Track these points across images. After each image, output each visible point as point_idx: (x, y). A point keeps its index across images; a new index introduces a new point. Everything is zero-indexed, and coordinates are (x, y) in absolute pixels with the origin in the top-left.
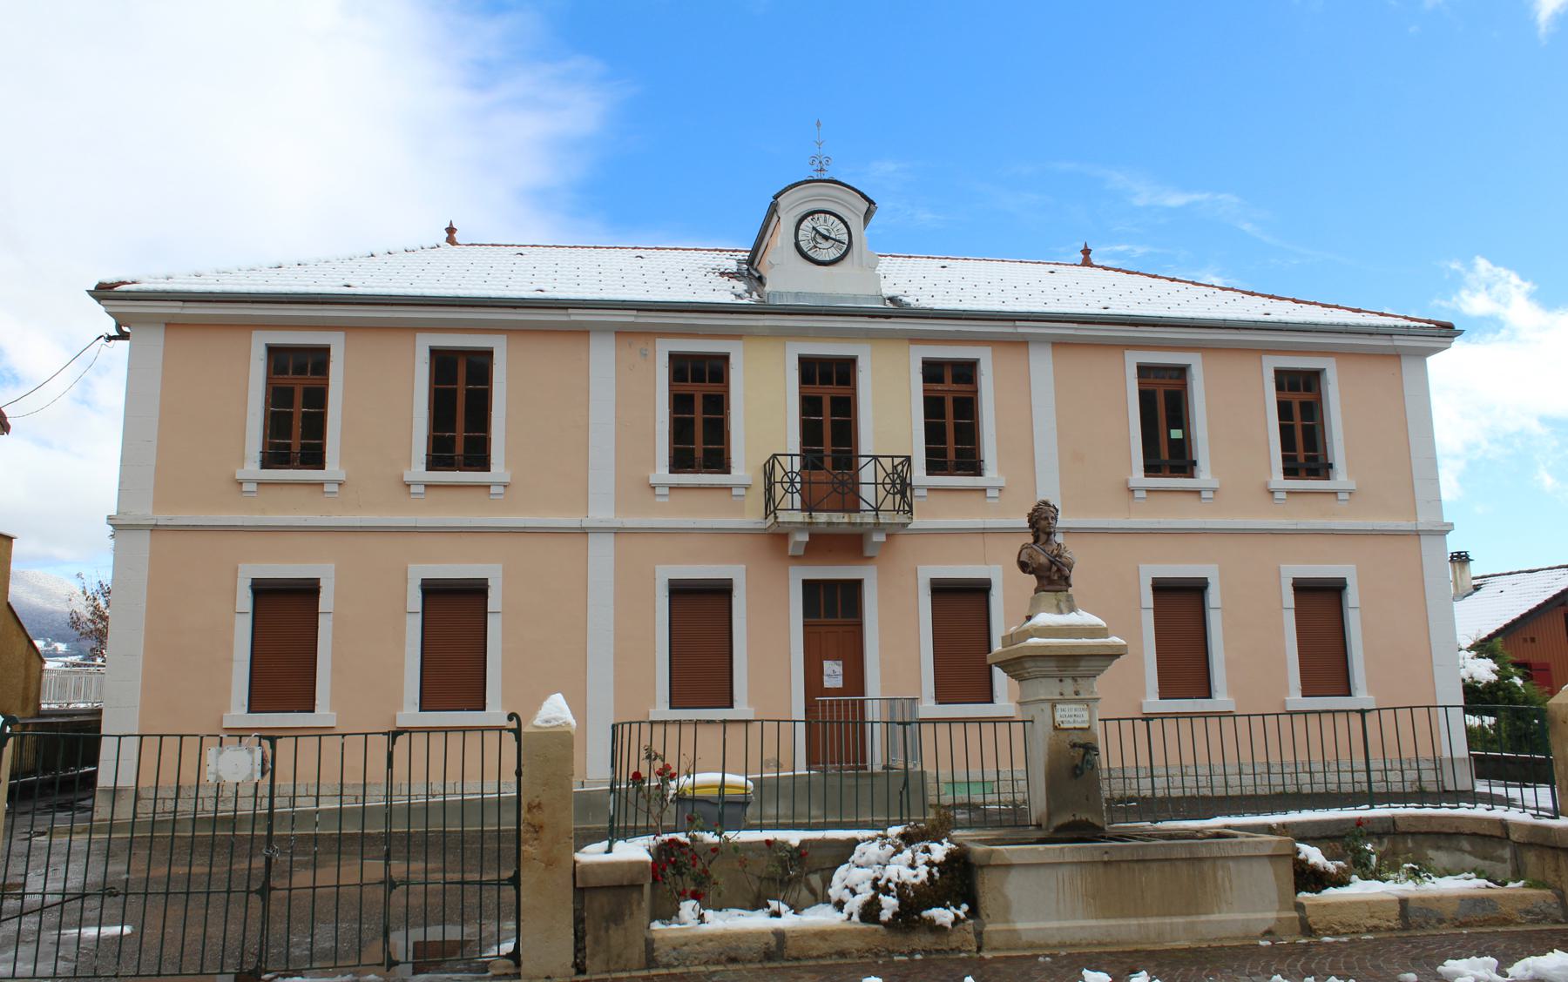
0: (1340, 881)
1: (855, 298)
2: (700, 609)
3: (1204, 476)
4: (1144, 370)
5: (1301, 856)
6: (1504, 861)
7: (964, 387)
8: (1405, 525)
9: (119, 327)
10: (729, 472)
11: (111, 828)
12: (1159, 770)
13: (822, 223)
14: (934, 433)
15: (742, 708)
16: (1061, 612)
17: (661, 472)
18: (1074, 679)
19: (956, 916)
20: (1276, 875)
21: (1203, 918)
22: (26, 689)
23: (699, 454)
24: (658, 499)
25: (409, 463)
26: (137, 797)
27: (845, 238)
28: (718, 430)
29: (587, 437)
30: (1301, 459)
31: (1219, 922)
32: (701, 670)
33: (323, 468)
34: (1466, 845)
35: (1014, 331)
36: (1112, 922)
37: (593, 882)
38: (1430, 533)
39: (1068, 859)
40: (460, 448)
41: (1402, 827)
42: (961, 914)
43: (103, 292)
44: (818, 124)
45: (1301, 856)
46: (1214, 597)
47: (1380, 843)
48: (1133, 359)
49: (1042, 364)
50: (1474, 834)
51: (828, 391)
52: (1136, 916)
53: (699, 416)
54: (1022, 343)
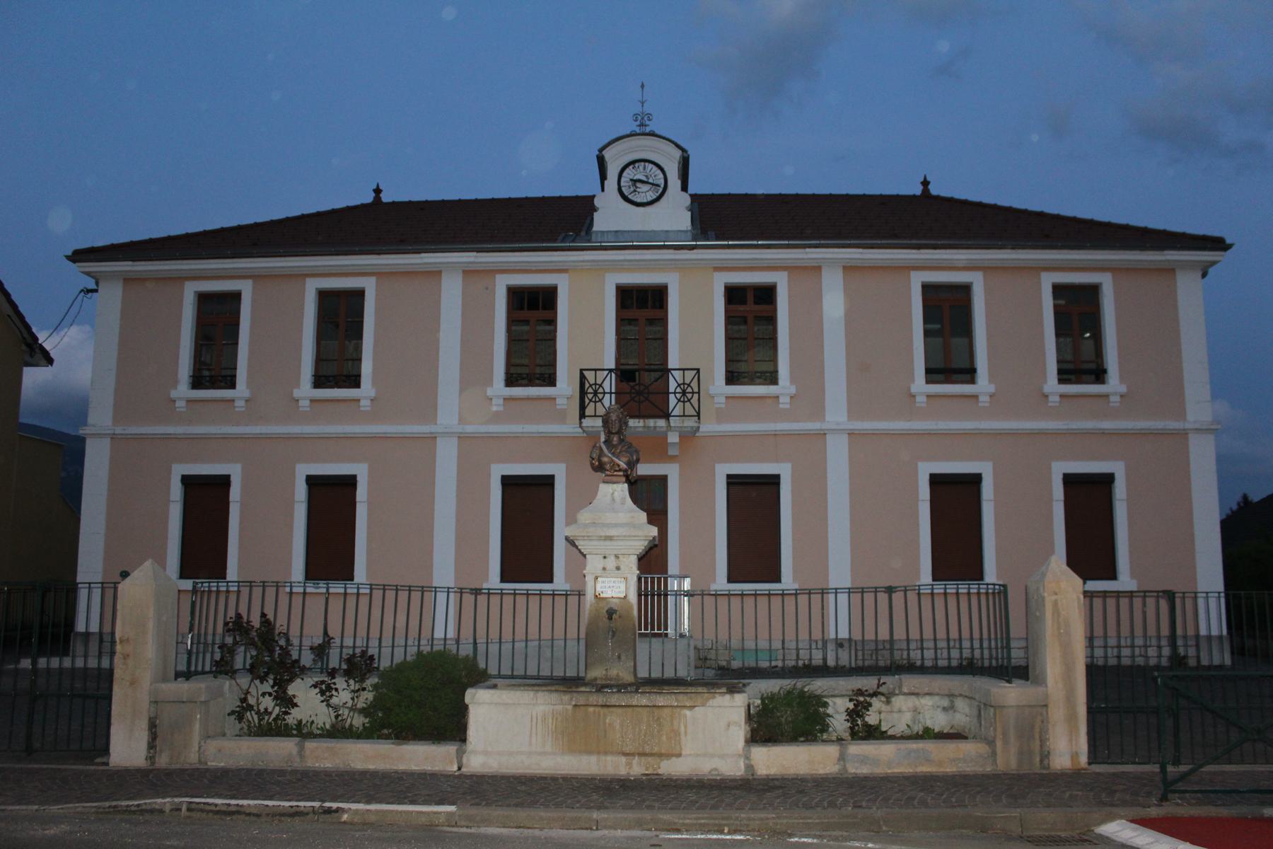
2: (528, 504)
9: (97, 283)
25: (175, 383)
26: (101, 641)
27: (662, 182)
44: (643, 86)
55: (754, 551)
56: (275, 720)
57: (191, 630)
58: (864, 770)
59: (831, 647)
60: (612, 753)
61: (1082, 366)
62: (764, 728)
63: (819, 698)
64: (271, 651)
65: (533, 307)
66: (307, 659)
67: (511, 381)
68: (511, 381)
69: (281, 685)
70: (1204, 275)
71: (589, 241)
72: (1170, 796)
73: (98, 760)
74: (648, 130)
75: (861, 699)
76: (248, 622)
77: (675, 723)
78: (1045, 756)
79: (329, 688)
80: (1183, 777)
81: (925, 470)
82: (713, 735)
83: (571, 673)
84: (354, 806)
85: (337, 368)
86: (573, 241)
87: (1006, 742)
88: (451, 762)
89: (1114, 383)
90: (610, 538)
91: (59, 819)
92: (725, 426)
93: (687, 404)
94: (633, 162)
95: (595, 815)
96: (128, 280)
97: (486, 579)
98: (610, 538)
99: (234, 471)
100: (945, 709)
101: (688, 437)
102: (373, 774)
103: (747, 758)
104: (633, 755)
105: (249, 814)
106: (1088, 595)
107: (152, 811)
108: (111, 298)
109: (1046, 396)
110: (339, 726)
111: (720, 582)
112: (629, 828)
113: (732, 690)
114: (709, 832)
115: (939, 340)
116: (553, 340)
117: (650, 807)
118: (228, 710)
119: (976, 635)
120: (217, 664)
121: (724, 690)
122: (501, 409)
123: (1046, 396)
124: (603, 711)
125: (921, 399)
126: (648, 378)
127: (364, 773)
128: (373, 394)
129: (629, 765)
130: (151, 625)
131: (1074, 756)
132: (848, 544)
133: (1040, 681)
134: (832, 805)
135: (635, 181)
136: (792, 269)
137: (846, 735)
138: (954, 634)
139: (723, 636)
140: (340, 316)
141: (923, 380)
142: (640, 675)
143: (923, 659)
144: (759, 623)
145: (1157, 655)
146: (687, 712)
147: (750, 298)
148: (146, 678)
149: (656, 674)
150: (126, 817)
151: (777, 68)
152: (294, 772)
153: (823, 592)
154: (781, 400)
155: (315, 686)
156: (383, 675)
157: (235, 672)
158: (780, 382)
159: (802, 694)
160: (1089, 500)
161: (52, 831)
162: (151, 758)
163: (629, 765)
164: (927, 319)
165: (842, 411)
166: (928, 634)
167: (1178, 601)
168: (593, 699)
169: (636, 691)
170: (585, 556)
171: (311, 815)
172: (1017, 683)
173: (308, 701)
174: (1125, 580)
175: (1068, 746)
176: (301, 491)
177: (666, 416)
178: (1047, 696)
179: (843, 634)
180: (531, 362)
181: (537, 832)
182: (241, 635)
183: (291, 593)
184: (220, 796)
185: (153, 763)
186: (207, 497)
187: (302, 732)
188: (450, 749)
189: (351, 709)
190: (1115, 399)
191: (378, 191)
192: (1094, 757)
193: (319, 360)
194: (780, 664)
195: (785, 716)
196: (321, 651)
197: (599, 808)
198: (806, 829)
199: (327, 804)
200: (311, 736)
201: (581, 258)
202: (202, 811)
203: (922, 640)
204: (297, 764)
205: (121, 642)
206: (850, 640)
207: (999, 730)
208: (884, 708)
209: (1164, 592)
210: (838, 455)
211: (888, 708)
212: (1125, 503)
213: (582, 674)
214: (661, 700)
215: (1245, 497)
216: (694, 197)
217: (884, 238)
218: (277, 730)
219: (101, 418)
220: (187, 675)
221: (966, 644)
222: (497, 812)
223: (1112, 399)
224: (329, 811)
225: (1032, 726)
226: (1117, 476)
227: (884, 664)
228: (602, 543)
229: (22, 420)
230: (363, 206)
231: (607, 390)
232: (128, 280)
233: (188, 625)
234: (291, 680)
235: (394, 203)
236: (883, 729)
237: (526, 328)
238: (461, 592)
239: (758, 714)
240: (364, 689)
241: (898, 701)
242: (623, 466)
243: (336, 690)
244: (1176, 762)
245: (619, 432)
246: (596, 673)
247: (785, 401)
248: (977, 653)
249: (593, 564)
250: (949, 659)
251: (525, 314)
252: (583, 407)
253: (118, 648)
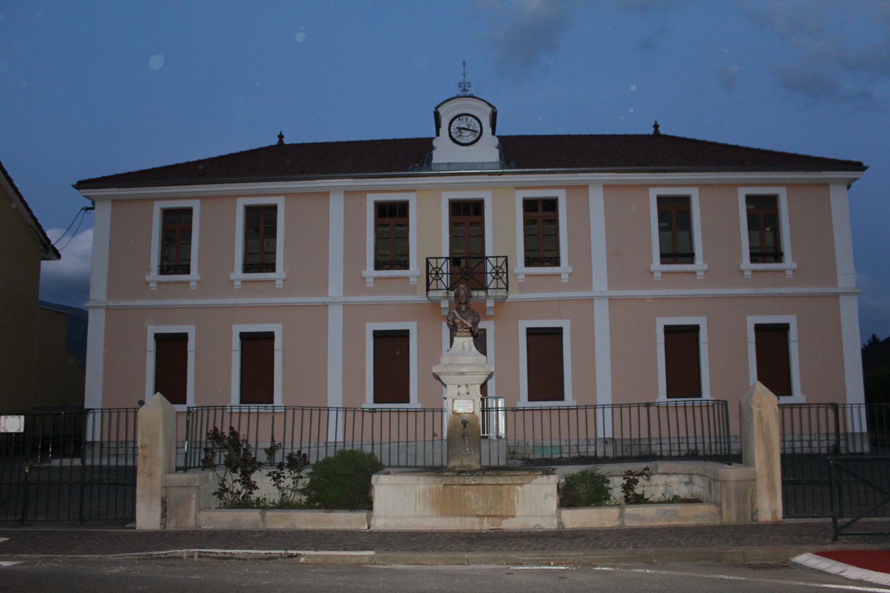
2: (391, 350)
8: (829, 290)
9: (93, 203)
10: (408, 268)
25: (148, 270)
26: (102, 447)
27: (479, 129)
44: (464, 64)
55: (546, 377)
56: (243, 497)
57: (187, 439)
58: (636, 524)
60: (470, 516)
61: (766, 250)
62: (569, 497)
63: (603, 477)
64: (239, 453)
65: (392, 215)
66: (262, 457)
67: (378, 266)
68: (378, 266)
69: (246, 475)
70: (849, 187)
71: (430, 170)
72: (839, 537)
73: (128, 526)
74: (468, 93)
75: (631, 477)
76: (222, 433)
77: (511, 494)
78: (755, 513)
79: (279, 476)
80: (848, 525)
81: (661, 322)
82: (535, 502)
83: (437, 463)
84: (308, 553)
85: (259, 260)
86: (419, 170)
87: (728, 504)
88: (363, 523)
89: (788, 262)
90: (462, 374)
91: (118, 565)
92: (526, 296)
93: (500, 281)
94: (459, 116)
95: (466, 555)
96: (115, 201)
97: (364, 401)
98: (462, 374)
99: (277, 329)
100: (686, 483)
101: (500, 303)
102: (313, 532)
103: (559, 517)
104: (483, 516)
105: (239, 559)
106: (781, 407)
107: (175, 558)
108: (104, 213)
109: (742, 272)
110: (285, 501)
111: (523, 401)
112: (489, 563)
113: (547, 473)
114: (541, 565)
115: (669, 234)
116: (406, 238)
117: (500, 550)
118: (213, 491)
119: (699, 433)
120: (204, 461)
121: (540, 473)
122: (372, 285)
123: (742, 272)
124: (463, 488)
125: (657, 275)
126: (474, 263)
127: (307, 531)
128: (284, 276)
129: (481, 523)
130: (161, 436)
131: (774, 513)
132: (607, 377)
133: (750, 464)
134: (619, 546)
135: (460, 129)
136: (570, 188)
137: (623, 502)
138: (683, 434)
139: (520, 437)
140: (261, 223)
141: (659, 262)
142: (483, 464)
143: (661, 451)
144: (550, 428)
145: (822, 446)
146: (519, 488)
147: (540, 208)
148: (159, 471)
149: (494, 463)
150: (157, 561)
151: (533, 43)
152: (260, 532)
153: (595, 407)
154: (563, 276)
155: (269, 475)
156: (314, 467)
157: (215, 466)
158: (562, 264)
159: (592, 475)
160: (772, 342)
161: (115, 571)
162: (163, 524)
163: (481, 523)
164: (661, 219)
165: (605, 283)
166: (665, 434)
167: (840, 410)
168: (457, 480)
169: (484, 475)
170: (445, 386)
171: (279, 559)
172: (734, 465)
173: (265, 486)
174: (798, 396)
175: (770, 506)
176: (236, 343)
177: (485, 289)
178: (755, 473)
179: (609, 435)
180: (392, 253)
181: (429, 567)
182: (217, 442)
183: (231, 413)
184: (217, 548)
185: (165, 528)
186: (172, 349)
187: (260, 505)
188: (363, 515)
189: (292, 490)
190: (789, 273)
191: (281, 136)
192: (786, 513)
193: (247, 254)
194: (577, 455)
195: (582, 490)
196: (271, 452)
197: (468, 551)
198: (604, 562)
199: (290, 552)
200: (265, 508)
201: (425, 182)
202: (208, 557)
203: (660, 438)
204: (261, 526)
205: (142, 447)
206: (613, 439)
207: (724, 496)
208: (646, 483)
209: (831, 404)
210: (601, 315)
211: (648, 483)
212: (797, 344)
213: (445, 464)
214: (501, 480)
215: (874, 337)
216: (499, 137)
217: (631, 165)
218: (245, 504)
219: (98, 294)
220: (185, 469)
221: (692, 440)
222: (403, 555)
223: (787, 273)
224: (291, 556)
225: (746, 493)
226: (791, 325)
227: (641, 455)
228: (457, 377)
229: (40, 298)
230: (271, 147)
231: (445, 271)
232: (115, 201)
233: (185, 436)
234: (253, 471)
235: (292, 144)
236: (646, 497)
237: (387, 229)
238: (345, 410)
239: (563, 488)
240: (301, 477)
241: (655, 479)
242: (470, 325)
243: (284, 477)
244: (841, 516)
245: (466, 303)
246: (455, 463)
247: (565, 278)
248: (700, 447)
249: (450, 391)
250: (679, 450)
251: (387, 220)
252: (428, 285)
253: (140, 451)
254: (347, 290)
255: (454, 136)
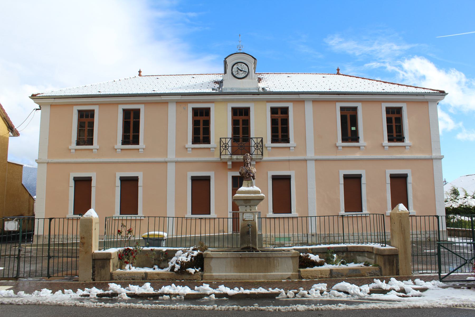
0: (321, 264)
1: (249, 89)
2: (201, 186)
3: (362, 142)
4: (342, 109)
5: (309, 257)
6: (372, 259)
7: (284, 115)
8: (427, 156)
9: (40, 107)
11: (37, 245)
12: (356, 234)
13: (240, 66)
14: (274, 130)
15: (213, 214)
16: (248, 187)
17: (189, 144)
18: (250, 206)
19: (196, 271)
20: (293, 263)
21: (269, 274)
22: (29, 208)
23: (201, 138)
24: (188, 152)
25: (71, 143)
28: (207, 131)
29: (169, 135)
30: (395, 135)
31: (274, 275)
32: (201, 203)
33: (92, 145)
34: (366, 255)
35: (300, 97)
36: (241, 274)
37: (97, 258)
38: (436, 159)
39: (229, 256)
40: (131, 138)
41: (349, 250)
42: (198, 270)
43: (33, 97)
45: (309, 257)
46: (363, 180)
47: (343, 254)
48: (339, 105)
49: (309, 107)
50: (368, 252)
51: (241, 117)
52: (249, 272)
53: (201, 127)
54: (303, 101)
59: (310, 236)
92: (272, 159)
94: (247, 66)
179: (314, 232)
231: (253, 147)
254: (178, 153)
255: (234, 73)
